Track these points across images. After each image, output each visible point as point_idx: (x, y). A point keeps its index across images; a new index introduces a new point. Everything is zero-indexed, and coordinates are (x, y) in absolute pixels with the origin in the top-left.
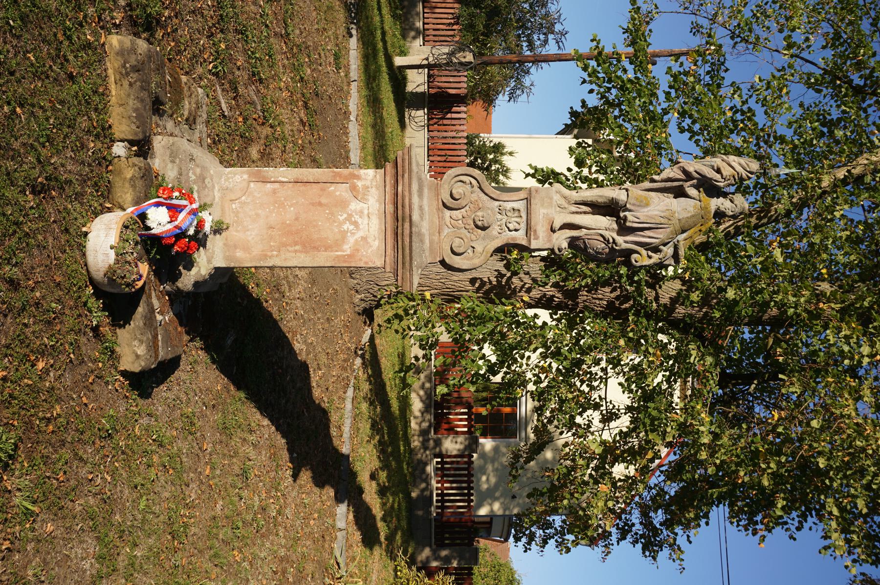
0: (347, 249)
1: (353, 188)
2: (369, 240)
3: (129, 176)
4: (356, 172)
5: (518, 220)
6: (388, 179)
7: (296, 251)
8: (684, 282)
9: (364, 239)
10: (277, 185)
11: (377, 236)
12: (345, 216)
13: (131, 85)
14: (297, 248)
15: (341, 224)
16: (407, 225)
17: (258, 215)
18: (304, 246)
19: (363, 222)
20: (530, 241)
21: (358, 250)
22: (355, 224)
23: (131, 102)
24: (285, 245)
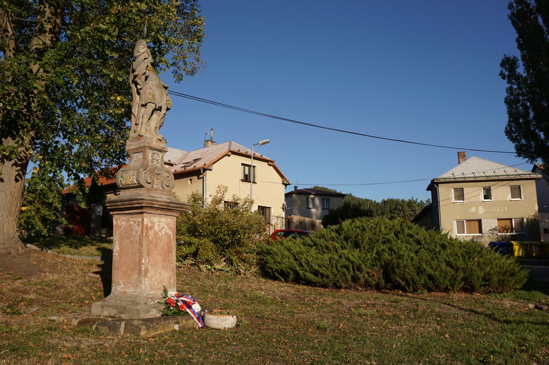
0: (170, 233)
3: (185, 322)
6: (149, 212)
8: (42, 67)
9: (168, 225)
10: (149, 264)
13: (157, 324)
15: (162, 235)
16: (171, 205)
18: (169, 252)
22: (163, 228)
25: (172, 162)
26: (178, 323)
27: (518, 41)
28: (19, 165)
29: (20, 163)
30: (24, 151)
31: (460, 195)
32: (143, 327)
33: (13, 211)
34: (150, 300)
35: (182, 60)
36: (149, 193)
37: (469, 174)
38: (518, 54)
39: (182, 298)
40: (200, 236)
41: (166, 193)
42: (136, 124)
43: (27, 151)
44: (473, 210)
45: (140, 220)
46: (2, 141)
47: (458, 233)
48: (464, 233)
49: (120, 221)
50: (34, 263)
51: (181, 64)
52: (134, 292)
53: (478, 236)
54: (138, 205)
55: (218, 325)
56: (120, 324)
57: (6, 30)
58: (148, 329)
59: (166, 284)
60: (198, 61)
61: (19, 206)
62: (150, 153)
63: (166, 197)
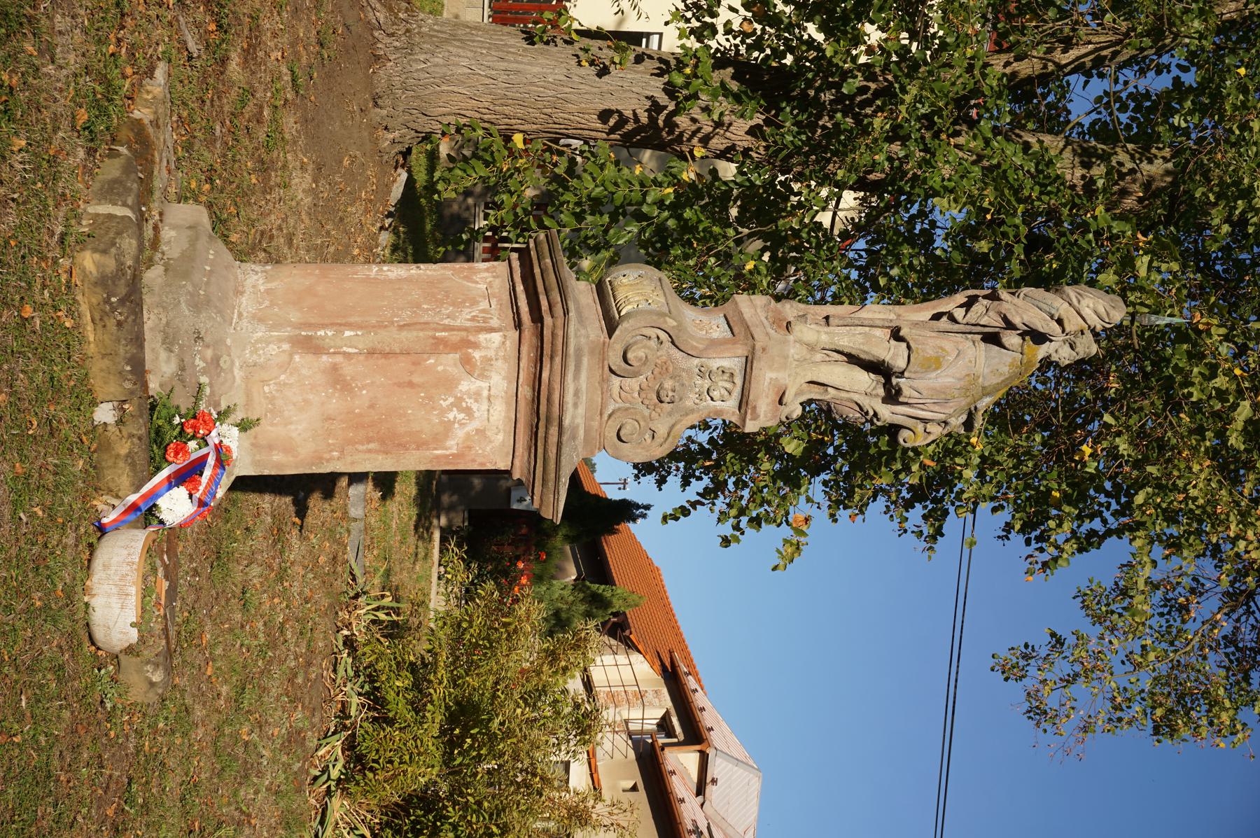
0: (453, 445)
1: (467, 362)
2: (488, 433)
3: (123, 451)
4: (471, 338)
5: (729, 386)
6: (524, 349)
7: (370, 451)
10: (339, 359)
11: (501, 427)
12: (451, 400)
13: (119, 324)
14: (372, 446)
15: (443, 411)
16: (554, 430)
17: (306, 401)
18: (382, 442)
19: (480, 409)
20: (744, 421)
21: (470, 448)
22: (468, 411)
23: (122, 351)
24: (351, 442)
25: (710, 789)
26: (120, 422)
28: (653, 120)
29: (661, 123)
30: (699, 130)
32: (110, 264)
33: (507, 110)
34: (209, 353)
35: (1078, 668)
36: (592, 352)
39: (211, 461)
40: (451, 744)
41: (595, 424)
42: (827, 318)
43: (700, 141)
45: (495, 322)
46: (724, 68)
49: (485, 283)
50: (346, 162)
51: (1062, 668)
52: (240, 315)
55: (106, 567)
56: (125, 205)
57: (1068, 44)
58: (104, 282)
59: (267, 430)
60: (1085, 730)
61: (526, 127)
62: (733, 363)
63: (580, 421)
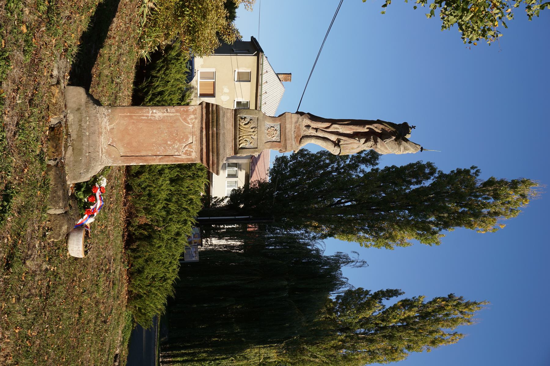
27: (393, 167)
31: (243, 78)
37: (265, 88)
38: (381, 165)
44: (226, 90)
47: (201, 72)
48: (201, 78)
53: (197, 94)
54: (211, 162)
56: (60, 208)
